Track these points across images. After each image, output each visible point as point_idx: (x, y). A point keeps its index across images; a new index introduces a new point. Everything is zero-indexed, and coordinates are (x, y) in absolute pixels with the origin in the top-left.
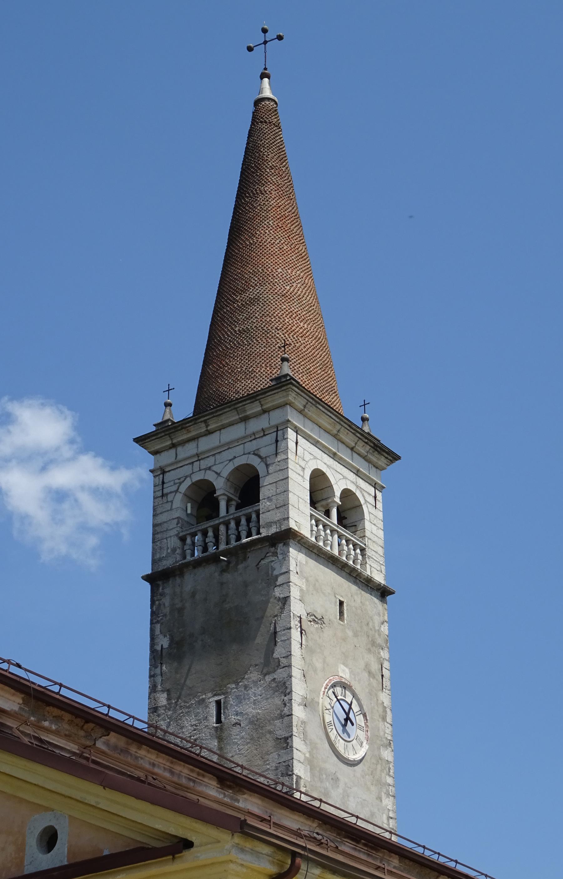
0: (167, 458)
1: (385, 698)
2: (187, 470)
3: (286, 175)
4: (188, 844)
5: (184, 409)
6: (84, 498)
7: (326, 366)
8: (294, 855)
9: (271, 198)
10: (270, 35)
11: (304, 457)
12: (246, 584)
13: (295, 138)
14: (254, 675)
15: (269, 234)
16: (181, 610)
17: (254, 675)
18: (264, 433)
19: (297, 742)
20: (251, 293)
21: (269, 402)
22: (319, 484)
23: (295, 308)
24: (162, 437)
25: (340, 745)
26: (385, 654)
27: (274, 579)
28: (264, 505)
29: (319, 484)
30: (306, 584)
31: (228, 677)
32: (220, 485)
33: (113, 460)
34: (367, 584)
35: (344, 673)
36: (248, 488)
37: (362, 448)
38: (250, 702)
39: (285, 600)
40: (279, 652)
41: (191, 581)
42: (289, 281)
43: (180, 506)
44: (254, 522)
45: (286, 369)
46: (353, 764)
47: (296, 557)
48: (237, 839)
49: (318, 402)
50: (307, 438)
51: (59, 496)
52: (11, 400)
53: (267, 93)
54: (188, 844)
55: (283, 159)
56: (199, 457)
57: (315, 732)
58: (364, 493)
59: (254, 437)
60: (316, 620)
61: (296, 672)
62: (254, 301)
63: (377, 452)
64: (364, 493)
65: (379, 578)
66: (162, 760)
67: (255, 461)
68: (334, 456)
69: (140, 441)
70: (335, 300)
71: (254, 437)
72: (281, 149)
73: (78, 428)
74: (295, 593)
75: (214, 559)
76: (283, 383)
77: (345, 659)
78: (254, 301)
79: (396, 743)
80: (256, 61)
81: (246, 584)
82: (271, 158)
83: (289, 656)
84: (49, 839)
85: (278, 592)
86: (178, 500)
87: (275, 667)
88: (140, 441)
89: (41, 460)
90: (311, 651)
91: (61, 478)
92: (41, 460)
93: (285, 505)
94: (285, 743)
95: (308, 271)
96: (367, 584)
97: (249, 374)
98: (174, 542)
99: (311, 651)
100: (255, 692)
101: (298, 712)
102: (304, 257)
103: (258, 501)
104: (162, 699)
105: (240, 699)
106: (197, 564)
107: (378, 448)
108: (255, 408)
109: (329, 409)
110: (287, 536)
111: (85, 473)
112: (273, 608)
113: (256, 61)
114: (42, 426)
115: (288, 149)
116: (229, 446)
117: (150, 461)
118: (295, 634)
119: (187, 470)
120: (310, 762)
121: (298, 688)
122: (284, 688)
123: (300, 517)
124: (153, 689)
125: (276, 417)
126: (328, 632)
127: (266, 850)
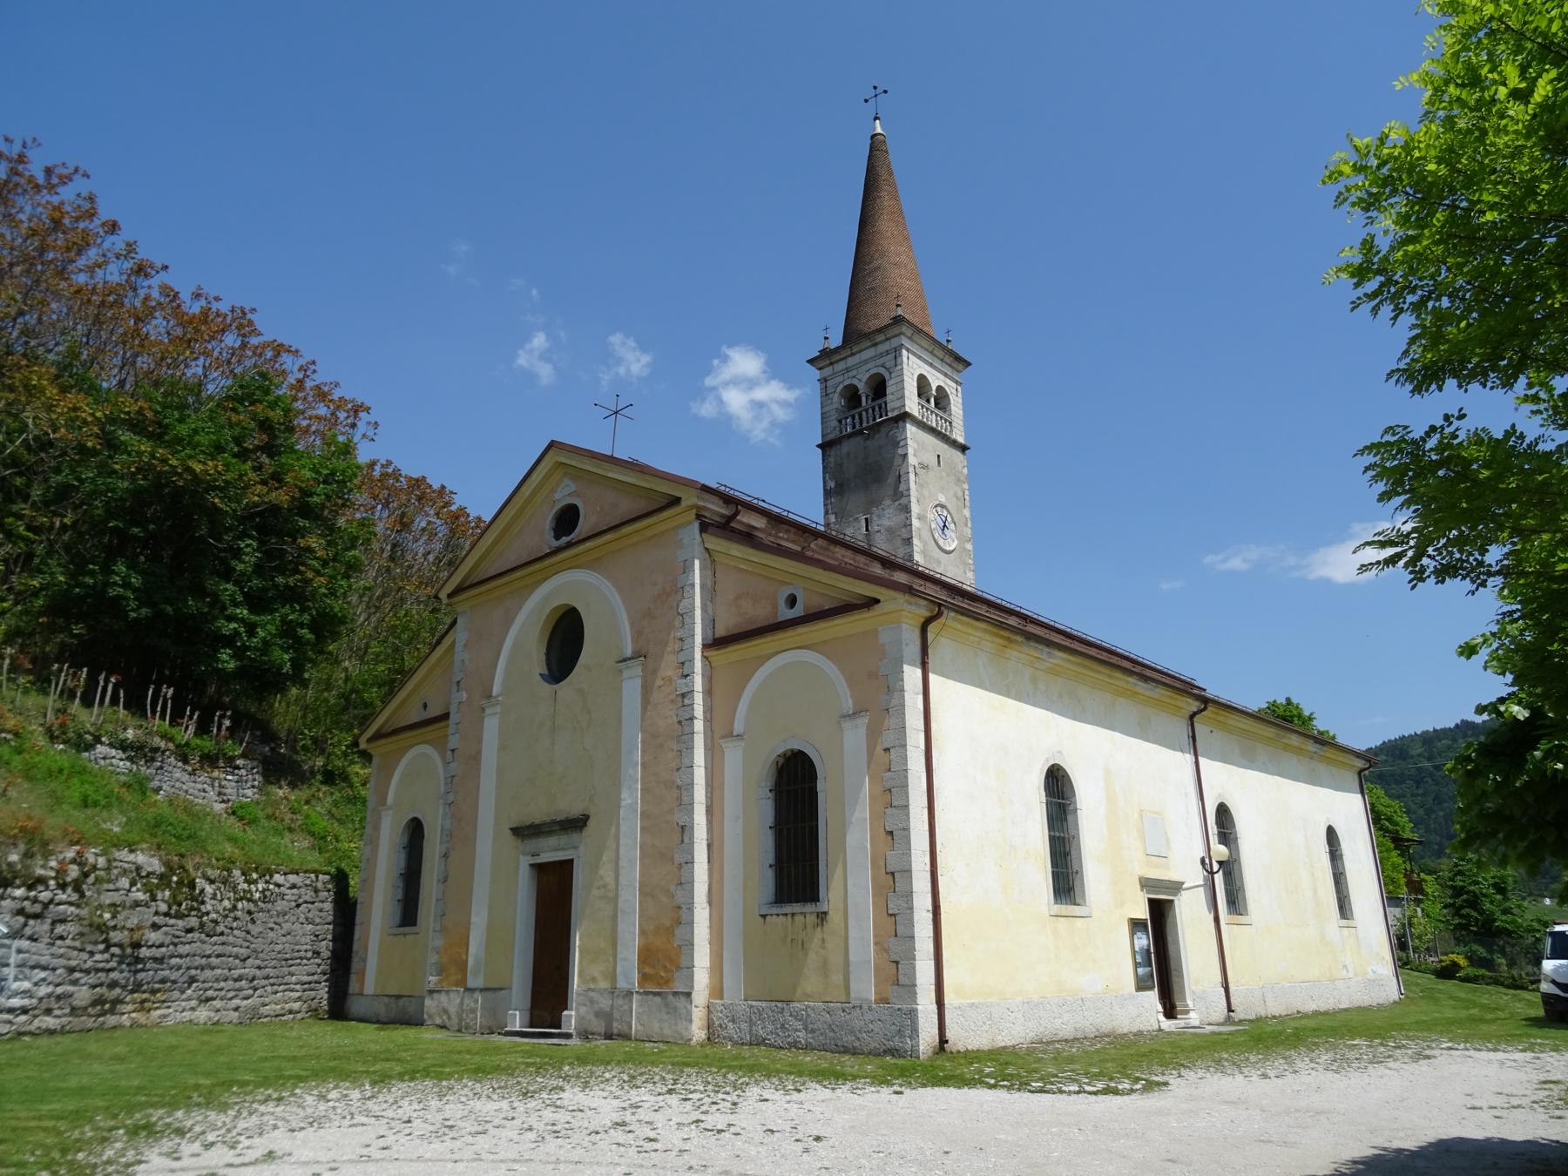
0: (828, 371)
1: (967, 512)
2: (840, 379)
3: (894, 185)
4: (877, 601)
5: (836, 340)
6: (775, 407)
7: (924, 308)
8: (940, 605)
9: (885, 200)
10: (879, 90)
11: (913, 366)
12: (880, 447)
13: (896, 157)
14: (888, 502)
15: (885, 225)
16: (841, 465)
17: (888, 502)
18: (888, 353)
19: (915, 541)
20: (875, 264)
21: (890, 333)
22: (922, 382)
23: (903, 271)
24: (824, 358)
25: (941, 542)
26: (966, 486)
27: (897, 443)
28: (889, 398)
29: (922, 382)
30: (917, 445)
31: (872, 504)
32: (861, 387)
33: (790, 383)
34: (954, 444)
35: (942, 499)
36: (879, 387)
37: (948, 359)
38: (886, 518)
39: (905, 456)
40: (902, 487)
41: (846, 447)
42: (898, 255)
43: (837, 401)
44: (883, 409)
45: (900, 311)
46: (949, 552)
47: (910, 429)
48: (907, 597)
49: (920, 331)
50: (914, 354)
51: (759, 405)
52: (730, 346)
53: (879, 130)
54: (877, 601)
55: (891, 174)
56: (848, 370)
57: (926, 534)
58: (950, 387)
59: (881, 355)
60: (924, 467)
61: (913, 499)
62: (877, 269)
63: (958, 362)
64: (950, 387)
65: (961, 440)
66: (849, 553)
67: (882, 371)
68: (931, 365)
69: (810, 361)
70: (921, 269)
71: (881, 355)
72: (889, 166)
73: (767, 363)
74: (910, 451)
75: (860, 432)
76: (898, 320)
77: (942, 490)
78: (877, 269)
79: (974, 539)
80: (870, 109)
81: (880, 447)
82: (883, 172)
83: (908, 490)
84: (792, 601)
85: (900, 451)
86: (836, 397)
87: (900, 496)
88: (810, 361)
89: (750, 383)
90: (921, 486)
91: (761, 394)
92: (750, 383)
93: (903, 397)
94: (908, 541)
95: (910, 248)
96: (954, 444)
97: (876, 316)
98: (835, 423)
99: (921, 486)
100: (889, 512)
101: (915, 523)
102: (906, 239)
103: (885, 395)
104: (832, 518)
105: (879, 517)
106: (850, 436)
107: (958, 359)
108: (881, 337)
109: (927, 335)
110: (905, 416)
111: (772, 392)
112: (898, 461)
113: (870, 109)
114: (745, 363)
115: (893, 167)
116: (866, 362)
117: (817, 374)
118: (912, 476)
119: (840, 379)
120: (924, 553)
121: (915, 509)
122: (906, 509)
123: (912, 405)
124: (826, 513)
125: (894, 343)
126: (931, 474)
127: (924, 603)
